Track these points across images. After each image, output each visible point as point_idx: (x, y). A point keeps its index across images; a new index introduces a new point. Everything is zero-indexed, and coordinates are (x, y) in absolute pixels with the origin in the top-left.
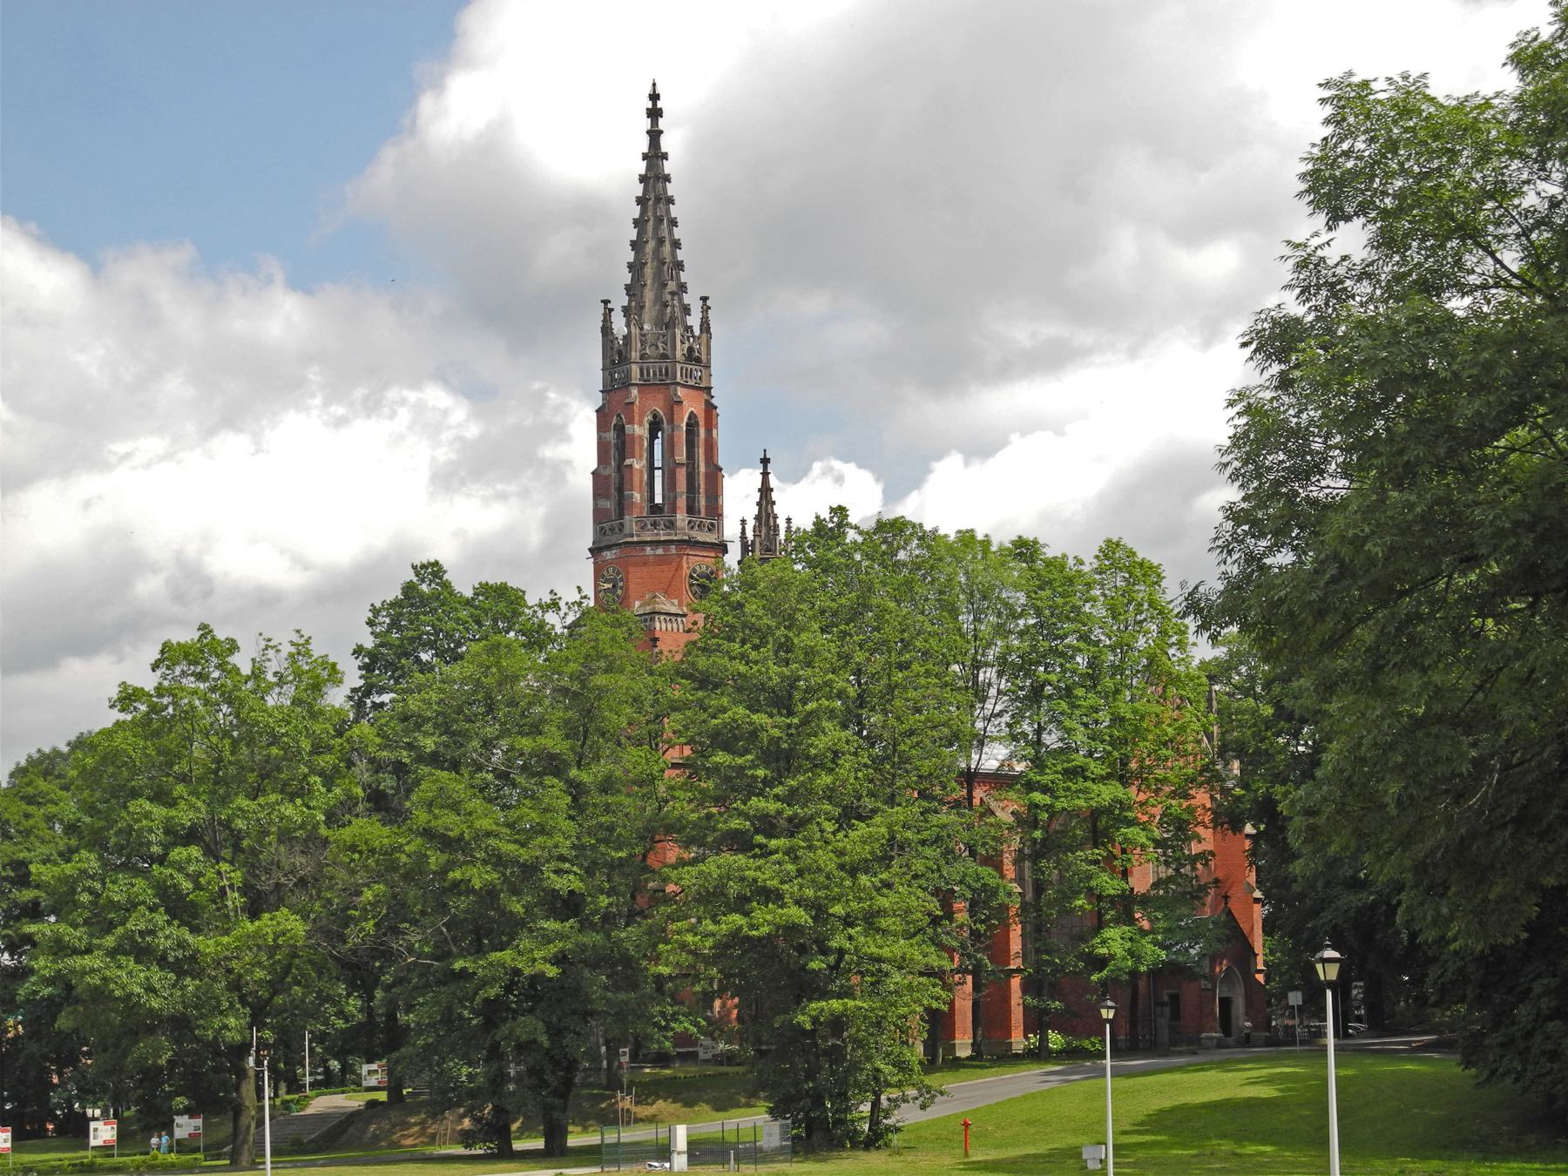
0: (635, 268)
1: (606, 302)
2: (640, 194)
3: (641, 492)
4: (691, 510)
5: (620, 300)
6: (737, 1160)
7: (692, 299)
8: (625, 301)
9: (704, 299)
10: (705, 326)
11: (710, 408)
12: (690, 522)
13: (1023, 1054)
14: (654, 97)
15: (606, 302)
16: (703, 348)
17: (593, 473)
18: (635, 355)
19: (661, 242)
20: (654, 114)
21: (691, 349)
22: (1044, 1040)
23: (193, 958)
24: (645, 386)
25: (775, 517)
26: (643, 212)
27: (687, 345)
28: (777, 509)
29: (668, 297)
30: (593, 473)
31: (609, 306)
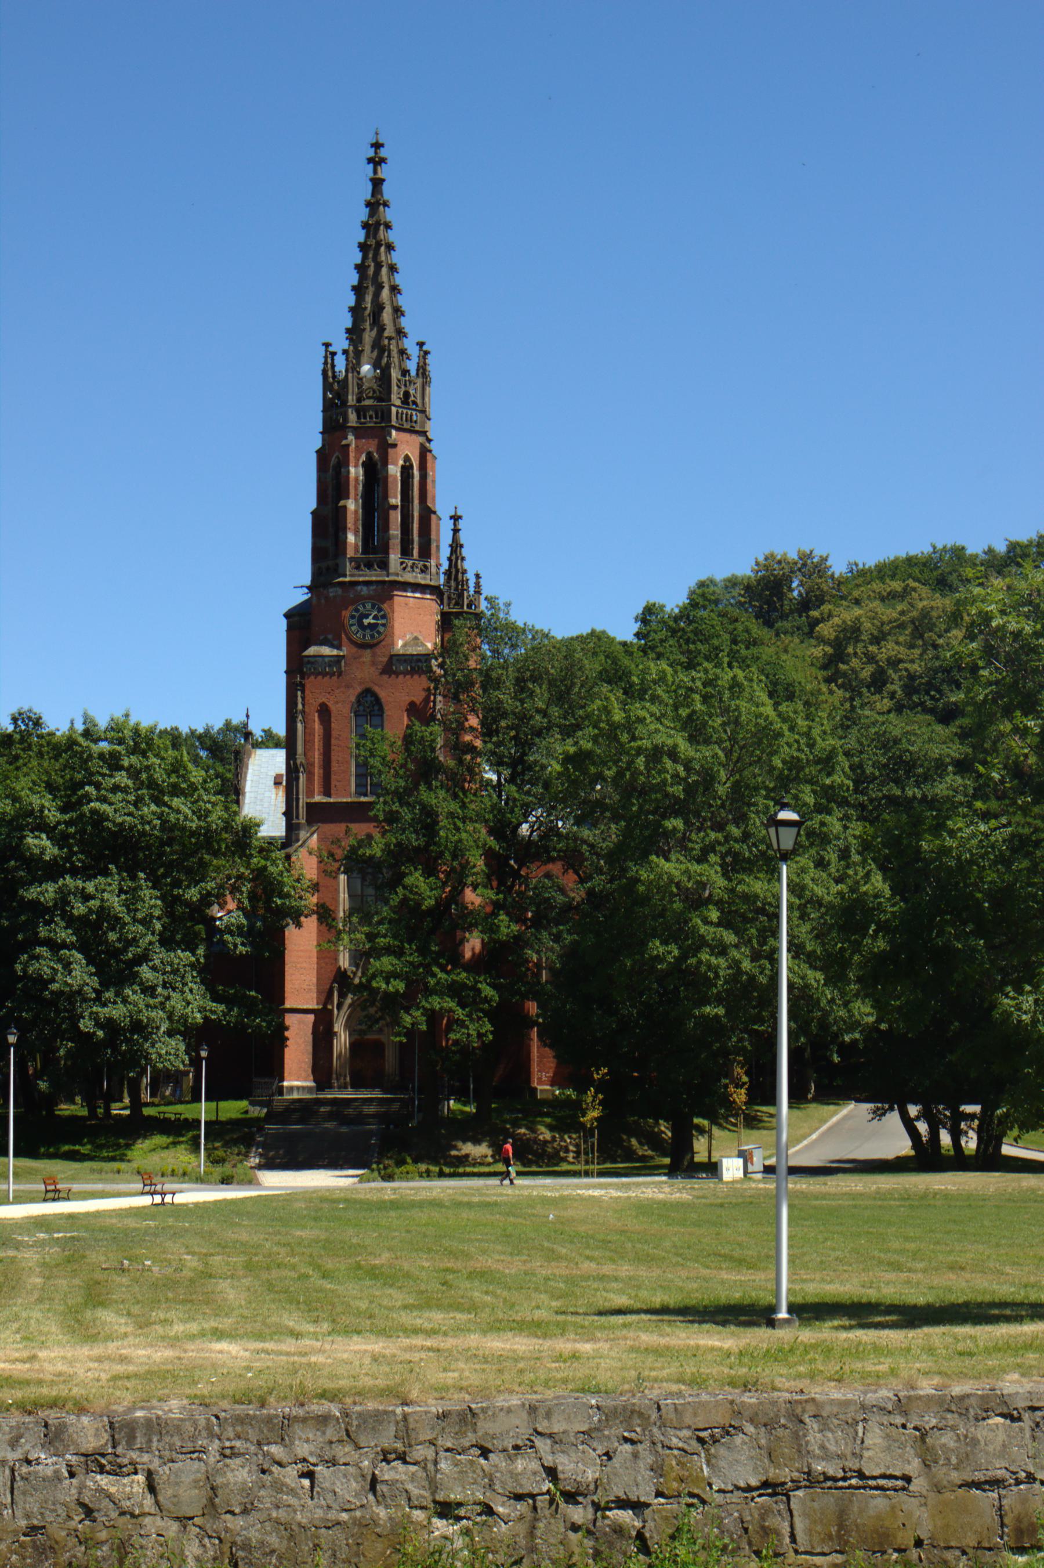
0: (356, 311)
1: (327, 345)
2: (359, 261)
3: (356, 534)
4: (406, 552)
5: (340, 343)
6: (639, 1347)
7: (410, 344)
8: (346, 344)
9: (421, 344)
10: (423, 370)
11: (424, 452)
12: (402, 563)
13: (733, 929)
14: (377, 146)
15: (327, 345)
16: (419, 395)
17: (317, 452)
18: (351, 400)
19: (380, 287)
20: (376, 162)
21: (407, 394)
22: (447, 965)
23: (999, 573)
24: (360, 433)
25: (465, 572)
26: (365, 258)
27: (403, 389)
28: (466, 565)
29: (386, 342)
30: (317, 452)
31: (331, 349)
